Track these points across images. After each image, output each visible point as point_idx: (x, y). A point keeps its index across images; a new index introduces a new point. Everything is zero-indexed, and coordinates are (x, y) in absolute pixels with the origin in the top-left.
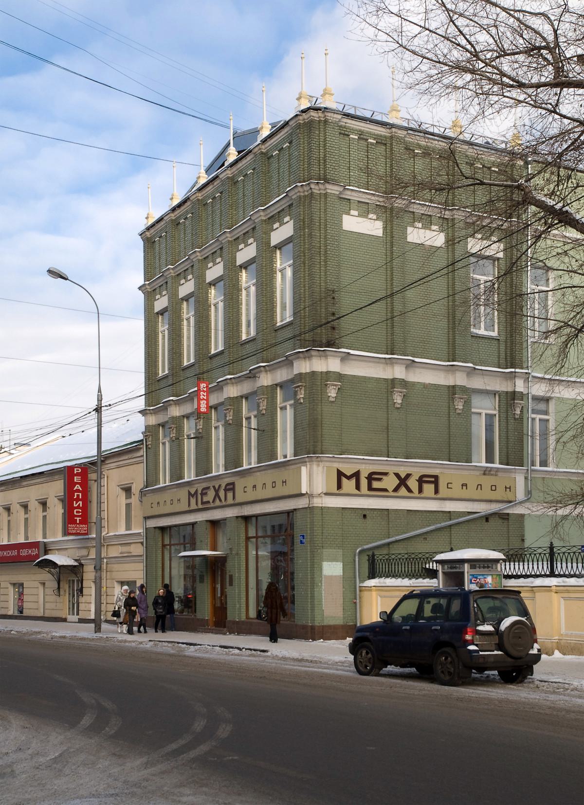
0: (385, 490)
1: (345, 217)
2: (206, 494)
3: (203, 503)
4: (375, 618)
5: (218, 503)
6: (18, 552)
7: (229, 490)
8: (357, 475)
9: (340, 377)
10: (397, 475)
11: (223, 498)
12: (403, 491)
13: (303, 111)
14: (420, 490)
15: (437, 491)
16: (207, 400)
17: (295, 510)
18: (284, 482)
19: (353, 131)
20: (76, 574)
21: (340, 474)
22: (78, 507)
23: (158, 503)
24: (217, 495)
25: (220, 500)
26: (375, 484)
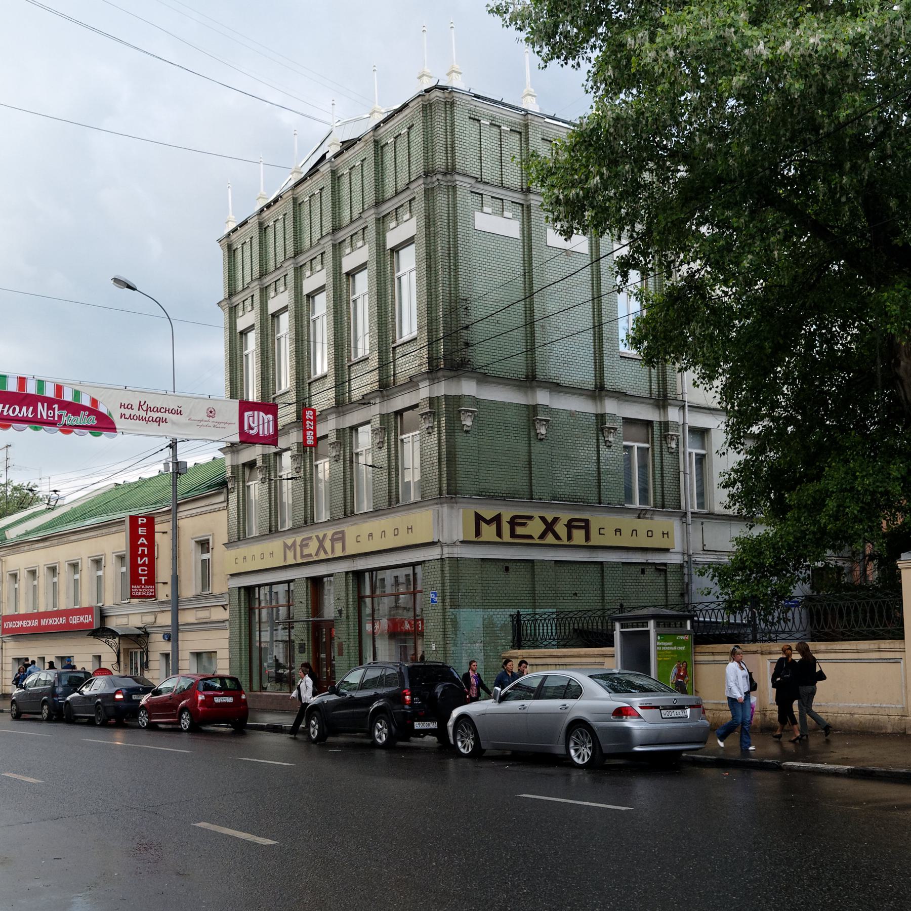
0: (530, 537)
1: (478, 215)
2: (307, 545)
3: (302, 556)
5: (322, 556)
6: (67, 620)
7: (338, 539)
8: (497, 519)
9: (476, 401)
10: (543, 519)
11: (329, 550)
13: (427, 91)
14: (570, 537)
15: (587, 538)
16: (315, 431)
18: (410, 529)
19: (485, 116)
21: (478, 518)
22: (144, 564)
23: (245, 558)
24: (321, 546)
25: (326, 552)
26: (519, 530)
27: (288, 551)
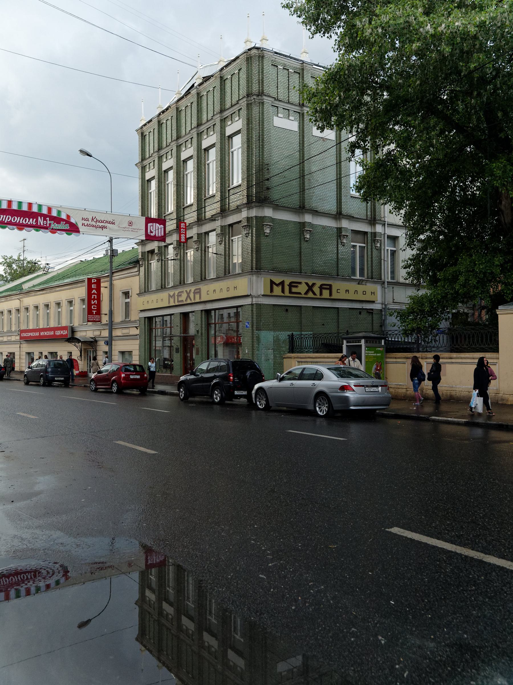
0: (300, 293)
2: (181, 295)
3: (178, 301)
4: (433, 392)
5: (189, 301)
7: (197, 293)
8: (282, 283)
9: (272, 220)
10: (307, 284)
11: (192, 299)
12: (310, 295)
14: (321, 294)
15: (331, 294)
16: (185, 234)
17: (242, 305)
20: (92, 346)
21: (272, 283)
22: (95, 304)
23: (148, 302)
25: (191, 300)
26: (294, 290)
27: (171, 298)
